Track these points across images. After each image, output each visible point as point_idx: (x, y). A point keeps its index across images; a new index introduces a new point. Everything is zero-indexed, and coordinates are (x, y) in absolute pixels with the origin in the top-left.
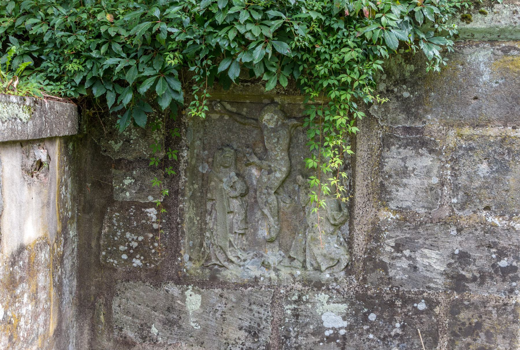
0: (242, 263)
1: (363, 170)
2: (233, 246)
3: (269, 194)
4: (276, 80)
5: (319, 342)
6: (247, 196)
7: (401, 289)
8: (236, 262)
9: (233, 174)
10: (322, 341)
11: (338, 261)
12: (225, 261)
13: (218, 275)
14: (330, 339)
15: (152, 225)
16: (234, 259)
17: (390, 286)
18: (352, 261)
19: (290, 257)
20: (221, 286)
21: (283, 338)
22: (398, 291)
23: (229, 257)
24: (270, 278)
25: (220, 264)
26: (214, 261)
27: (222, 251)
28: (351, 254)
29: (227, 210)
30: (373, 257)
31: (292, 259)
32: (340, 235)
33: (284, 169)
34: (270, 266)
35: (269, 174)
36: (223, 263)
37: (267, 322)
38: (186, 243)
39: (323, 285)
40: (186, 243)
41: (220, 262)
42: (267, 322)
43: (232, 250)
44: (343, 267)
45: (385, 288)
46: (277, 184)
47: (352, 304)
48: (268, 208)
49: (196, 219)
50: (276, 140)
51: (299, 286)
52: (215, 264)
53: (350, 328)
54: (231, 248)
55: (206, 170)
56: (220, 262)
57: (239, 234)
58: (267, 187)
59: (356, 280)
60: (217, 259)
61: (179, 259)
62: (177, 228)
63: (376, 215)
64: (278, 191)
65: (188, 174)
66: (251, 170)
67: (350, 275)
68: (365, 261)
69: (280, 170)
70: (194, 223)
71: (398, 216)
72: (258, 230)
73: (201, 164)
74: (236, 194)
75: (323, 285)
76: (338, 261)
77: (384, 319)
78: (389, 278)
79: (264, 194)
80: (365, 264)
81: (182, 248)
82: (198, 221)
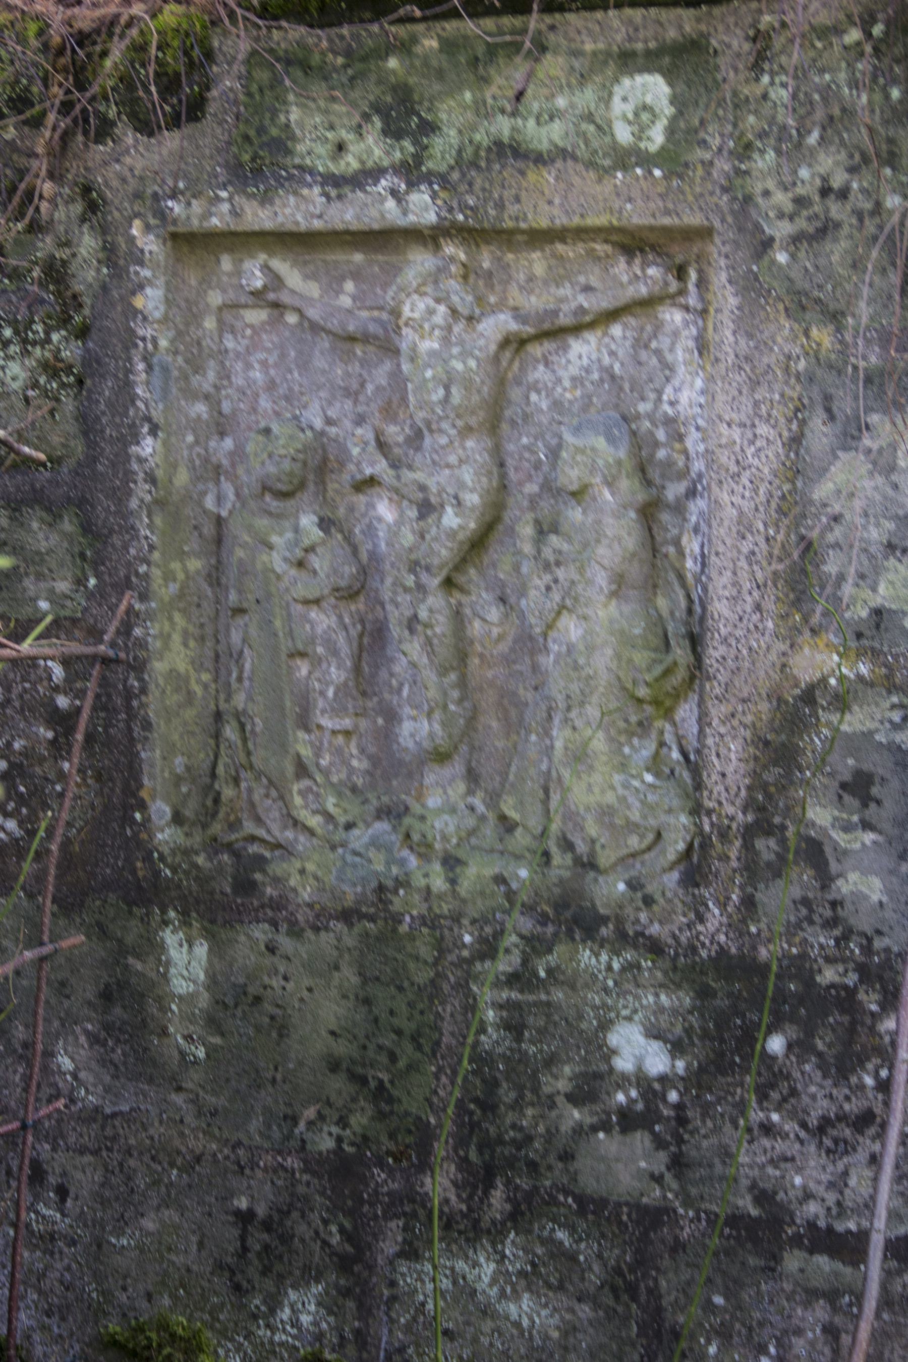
0: (340, 835)
1: (737, 500)
2: (311, 777)
3: (420, 587)
4: (580, 167)
5: (594, 1129)
6: (362, 598)
7: (878, 944)
8: (319, 831)
9: (308, 521)
10: (605, 1126)
11: (659, 835)
12: (285, 827)
13: (258, 876)
14: (628, 1121)
15: (53, 700)
16: (314, 821)
17: (837, 932)
18: (700, 831)
19: (503, 818)
20: (270, 913)
21: (472, 1106)
22: (867, 950)
23: (295, 813)
24: (428, 889)
25: (269, 838)
26: (249, 827)
27: (274, 793)
28: (696, 810)
29: (285, 645)
30: (777, 820)
31: (507, 825)
32: (668, 737)
33: (472, 499)
34: (430, 846)
35: (422, 517)
36: (277, 833)
37: (419, 1047)
38: (159, 763)
39: (604, 920)
40: (159, 763)
41: (269, 831)
42: (419, 1047)
43: (309, 789)
44: (671, 856)
45: (822, 940)
46: (444, 552)
47: (704, 993)
48: (422, 639)
49: (199, 681)
50: (441, 392)
51: (526, 924)
52: (253, 839)
53: (696, 1081)
54: (306, 783)
55: (229, 505)
56: (269, 831)
57: (334, 732)
58: (417, 563)
59: (718, 903)
60: (259, 820)
61: (138, 816)
62: (129, 708)
63: (784, 666)
64: (461, 579)
65: (158, 521)
66: (373, 507)
67: (697, 885)
68: (749, 833)
69: (459, 503)
70: (190, 694)
71: (863, 669)
72: (400, 721)
73: (211, 485)
74: (320, 585)
75: (604, 920)
76: (659, 835)
77: (820, 1055)
78: (834, 904)
79: (406, 590)
80: (748, 846)
81: (146, 781)
82: (206, 687)
